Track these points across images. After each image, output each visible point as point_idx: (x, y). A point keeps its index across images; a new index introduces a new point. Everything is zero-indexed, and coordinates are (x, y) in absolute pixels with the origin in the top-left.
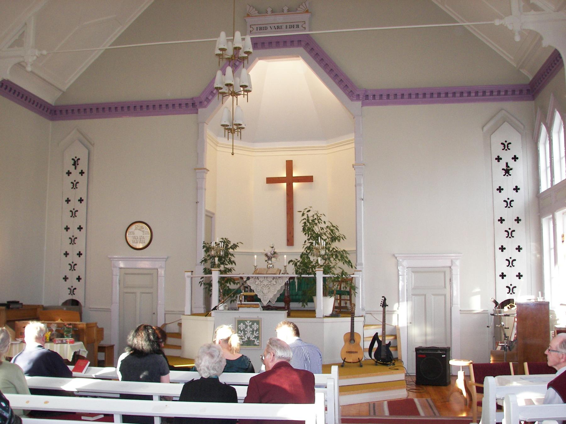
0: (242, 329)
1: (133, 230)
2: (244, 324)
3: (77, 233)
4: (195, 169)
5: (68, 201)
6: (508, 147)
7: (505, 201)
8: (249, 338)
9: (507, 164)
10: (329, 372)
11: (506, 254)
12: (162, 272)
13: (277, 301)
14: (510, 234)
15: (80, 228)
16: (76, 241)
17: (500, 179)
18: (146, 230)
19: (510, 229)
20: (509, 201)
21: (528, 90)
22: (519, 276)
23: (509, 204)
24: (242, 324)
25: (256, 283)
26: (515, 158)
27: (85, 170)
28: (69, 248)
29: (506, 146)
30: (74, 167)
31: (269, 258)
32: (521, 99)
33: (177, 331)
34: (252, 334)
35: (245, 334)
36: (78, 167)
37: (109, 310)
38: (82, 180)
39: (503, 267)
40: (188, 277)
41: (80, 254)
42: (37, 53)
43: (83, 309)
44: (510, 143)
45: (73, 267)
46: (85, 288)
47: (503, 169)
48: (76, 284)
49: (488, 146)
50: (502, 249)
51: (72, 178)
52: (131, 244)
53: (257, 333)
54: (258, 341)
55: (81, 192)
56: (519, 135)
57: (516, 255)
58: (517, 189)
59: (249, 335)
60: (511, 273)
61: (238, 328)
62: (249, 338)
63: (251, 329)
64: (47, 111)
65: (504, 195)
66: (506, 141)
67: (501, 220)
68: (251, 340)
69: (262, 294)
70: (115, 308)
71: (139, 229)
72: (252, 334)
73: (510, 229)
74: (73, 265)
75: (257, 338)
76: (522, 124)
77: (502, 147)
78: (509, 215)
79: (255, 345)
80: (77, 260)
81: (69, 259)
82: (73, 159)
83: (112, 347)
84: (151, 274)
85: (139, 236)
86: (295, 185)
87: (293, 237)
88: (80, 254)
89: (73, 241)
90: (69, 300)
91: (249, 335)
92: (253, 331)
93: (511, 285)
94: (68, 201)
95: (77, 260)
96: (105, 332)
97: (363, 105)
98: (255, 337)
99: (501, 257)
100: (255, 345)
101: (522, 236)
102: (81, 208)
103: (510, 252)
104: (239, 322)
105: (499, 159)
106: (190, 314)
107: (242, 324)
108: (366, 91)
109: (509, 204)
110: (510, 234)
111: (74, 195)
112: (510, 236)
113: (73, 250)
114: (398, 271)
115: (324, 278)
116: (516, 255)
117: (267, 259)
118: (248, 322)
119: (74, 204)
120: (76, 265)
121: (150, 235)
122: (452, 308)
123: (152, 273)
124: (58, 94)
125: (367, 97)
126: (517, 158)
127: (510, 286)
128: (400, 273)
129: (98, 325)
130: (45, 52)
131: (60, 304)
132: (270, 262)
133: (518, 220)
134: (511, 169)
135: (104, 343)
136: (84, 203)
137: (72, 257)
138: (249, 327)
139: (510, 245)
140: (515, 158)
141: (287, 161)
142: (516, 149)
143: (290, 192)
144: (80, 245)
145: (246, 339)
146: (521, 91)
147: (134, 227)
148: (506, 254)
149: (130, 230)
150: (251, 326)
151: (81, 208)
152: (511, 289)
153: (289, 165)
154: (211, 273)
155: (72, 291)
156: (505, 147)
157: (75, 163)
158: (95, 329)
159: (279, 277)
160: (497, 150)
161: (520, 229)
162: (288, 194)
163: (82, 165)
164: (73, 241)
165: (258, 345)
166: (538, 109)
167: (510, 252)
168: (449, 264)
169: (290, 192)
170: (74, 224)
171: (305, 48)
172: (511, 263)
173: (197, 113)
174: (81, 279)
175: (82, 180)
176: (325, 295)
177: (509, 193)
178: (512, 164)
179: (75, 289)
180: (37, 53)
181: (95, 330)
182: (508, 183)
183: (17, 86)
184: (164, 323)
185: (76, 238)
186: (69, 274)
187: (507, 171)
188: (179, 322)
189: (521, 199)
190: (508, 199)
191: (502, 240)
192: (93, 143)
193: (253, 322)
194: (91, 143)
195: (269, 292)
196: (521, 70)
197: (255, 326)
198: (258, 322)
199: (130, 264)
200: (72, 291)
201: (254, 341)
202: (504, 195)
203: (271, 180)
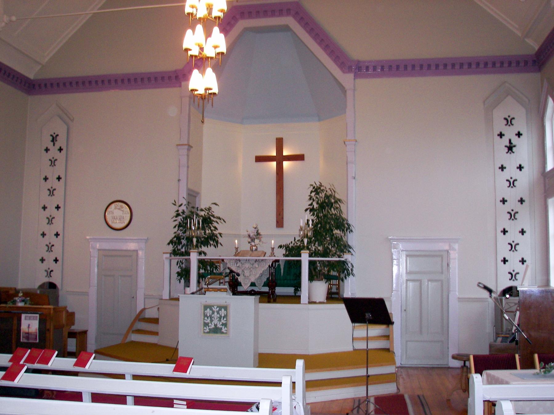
0: (208, 315)
2: (211, 309)
4: (177, 145)
5: (46, 179)
6: (513, 184)
7: (507, 180)
8: (216, 325)
9: (510, 141)
10: (293, 366)
11: (509, 238)
13: (263, 286)
14: (512, 216)
15: (58, 208)
16: (54, 221)
19: (512, 210)
21: (534, 62)
23: (512, 183)
24: (208, 310)
25: (238, 265)
26: (519, 135)
27: (64, 147)
29: (509, 121)
31: (253, 240)
32: (528, 72)
33: (156, 316)
34: (220, 320)
35: (211, 321)
36: (56, 143)
37: (86, 294)
38: (61, 157)
39: (504, 251)
40: (166, 258)
41: (57, 235)
42: (6, 18)
43: (61, 293)
44: (513, 118)
47: (506, 146)
48: (53, 266)
49: (489, 121)
50: (504, 232)
51: (50, 155)
52: (110, 223)
53: (225, 319)
54: (226, 329)
55: (59, 170)
56: (524, 110)
57: (519, 238)
58: (520, 168)
60: (514, 258)
61: (204, 313)
62: (216, 325)
63: (218, 315)
64: (16, 81)
65: (506, 174)
67: (504, 201)
68: (218, 328)
70: (93, 292)
71: (119, 209)
72: (220, 320)
74: (50, 246)
76: (526, 97)
78: (512, 195)
79: (223, 333)
80: (54, 240)
81: (46, 240)
82: (51, 135)
83: (85, 332)
84: (131, 256)
85: (119, 216)
86: (286, 164)
87: (283, 218)
88: (57, 235)
89: (50, 221)
91: (216, 321)
92: (220, 317)
93: (514, 271)
94: (46, 179)
95: (54, 240)
96: (77, 316)
97: (356, 77)
98: (223, 324)
99: (503, 241)
100: (223, 333)
101: (525, 219)
102: (59, 186)
103: (513, 236)
104: (206, 307)
105: (501, 135)
106: (168, 298)
107: (208, 310)
108: (359, 62)
109: (512, 183)
110: (512, 216)
113: (50, 231)
114: (392, 254)
116: (519, 238)
117: (250, 240)
118: (215, 307)
119: (53, 182)
120: (53, 245)
121: (129, 215)
123: (132, 255)
124: (38, 68)
125: (359, 68)
127: (512, 272)
128: (394, 257)
129: (67, 309)
130: (14, 18)
131: (36, 287)
132: (253, 244)
133: (522, 201)
134: (515, 146)
135: (77, 327)
136: (62, 181)
137: (50, 238)
138: (216, 313)
139: (513, 228)
140: (519, 135)
141: (277, 139)
142: (520, 125)
143: (280, 168)
144: (58, 226)
145: (213, 326)
146: (526, 63)
147: (113, 206)
148: (509, 238)
149: (109, 210)
150: (218, 313)
151: (59, 186)
152: (513, 276)
153: (280, 144)
154: (189, 255)
155: (49, 273)
157: (54, 139)
158: (64, 312)
159: (262, 260)
160: (500, 125)
161: (523, 211)
162: (277, 174)
163: (61, 142)
165: (226, 333)
166: (545, 80)
167: (513, 236)
169: (280, 168)
170: (51, 203)
172: (513, 247)
173: (180, 86)
176: (311, 278)
177: (511, 172)
179: (52, 271)
180: (6, 18)
181: (64, 315)
182: (511, 161)
183: (7, 67)
184: (143, 307)
185: (54, 218)
186: (46, 255)
187: (510, 148)
189: (525, 179)
192: (72, 118)
193: (220, 307)
194: (70, 119)
195: (252, 275)
196: (526, 40)
197: (223, 312)
198: (226, 308)
199: (106, 246)
200: (49, 273)
202: (506, 174)
203: (260, 159)
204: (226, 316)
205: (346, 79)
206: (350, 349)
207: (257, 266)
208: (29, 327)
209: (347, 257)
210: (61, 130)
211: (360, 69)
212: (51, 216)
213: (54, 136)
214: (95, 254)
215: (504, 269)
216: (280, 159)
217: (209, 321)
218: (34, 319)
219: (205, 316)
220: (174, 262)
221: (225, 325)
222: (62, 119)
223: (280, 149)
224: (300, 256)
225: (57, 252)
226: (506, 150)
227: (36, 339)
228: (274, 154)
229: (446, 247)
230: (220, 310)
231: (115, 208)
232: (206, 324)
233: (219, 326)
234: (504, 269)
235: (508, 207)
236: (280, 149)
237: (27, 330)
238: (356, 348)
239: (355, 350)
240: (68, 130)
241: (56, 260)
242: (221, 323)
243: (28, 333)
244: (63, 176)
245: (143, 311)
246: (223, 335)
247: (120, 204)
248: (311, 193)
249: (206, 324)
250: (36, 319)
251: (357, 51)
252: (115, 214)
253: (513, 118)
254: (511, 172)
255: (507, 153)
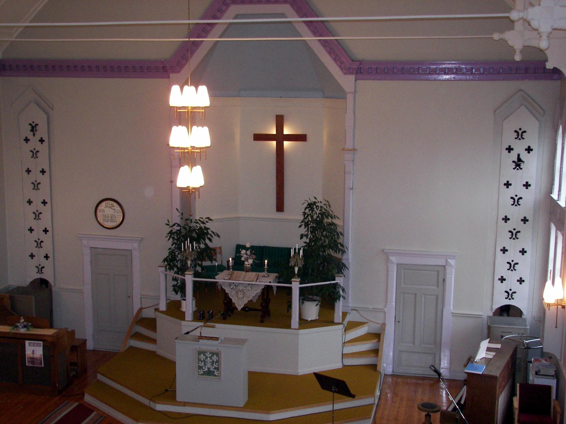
0: (202, 359)
1: (102, 208)
2: (204, 355)
3: (41, 207)
7: (512, 198)
8: (209, 369)
9: (519, 155)
11: (508, 257)
12: (136, 254)
14: (514, 234)
16: (40, 186)
17: (510, 173)
18: (117, 209)
19: (514, 229)
20: (516, 198)
22: (521, 281)
23: (516, 201)
24: (202, 355)
26: (523, 252)
27: (45, 138)
28: (33, 224)
29: (520, 135)
30: (32, 133)
34: (212, 365)
35: (205, 365)
36: (37, 133)
38: (43, 149)
39: (502, 270)
43: (54, 289)
45: (39, 244)
46: (53, 241)
47: (514, 162)
50: (504, 250)
55: (44, 193)
57: (518, 258)
58: (527, 185)
59: (209, 365)
61: (198, 358)
62: (209, 369)
65: (511, 192)
66: (520, 129)
67: (506, 219)
69: (236, 298)
70: (87, 288)
71: (110, 207)
72: (212, 365)
73: (514, 229)
74: (37, 213)
75: (217, 369)
77: (515, 135)
78: (516, 214)
79: (215, 376)
80: (43, 236)
81: (35, 236)
82: (30, 124)
86: (286, 144)
89: (37, 215)
90: (37, 279)
91: (209, 365)
92: (213, 362)
95: (43, 236)
98: (215, 368)
99: (502, 260)
100: (215, 376)
102: (44, 180)
103: (513, 255)
104: (200, 353)
105: (510, 149)
107: (202, 355)
109: (516, 201)
110: (514, 234)
111: (36, 165)
112: (514, 237)
113: (38, 227)
115: (301, 289)
116: (518, 258)
119: (36, 176)
120: (39, 183)
121: (121, 214)
122: (444, 310)
123: (127, 255)
126: (532, 150)
127: (509, 291)
136: (47, 174)
138: (209, 359)
140: (529, 150)
142: (530, 139)
143: (280, 147)
144: (45, 221)
145: (206, 369)
147: (104, 204)
148: (508, 257)
149: (100, 208)
150: (211, 358)
151: (44, 180)
153: (280, 122)
155: (40, 269)
156: (518, 135)
157: (33, 128)
160: (509, 139)
163: (42, 132)
164: (37, 215)
167: (513, 255)
168: (444, 264)
169: (280, 147)
171: (292, 5)
172: (512, 266)
173: (169, 78)
174: (49, 257)
175: (43, 149)
177: (517, 189)
178: (524, 156)
182: (518, 178)
186: (35, 251)
187: (518, 163)
188: (157, 307)
189: (529, 198)
190: (516, 196)
191: (505, 241)
192: (52, 106)
193: (213, 354)
197: (215, 358)
198: (217, 354)
200: (40, 269)
201: (214, 372)
202: (511, 192)
204: (217, 362)
205: (347, 81)
206: (339, 365)
207: (250, 289)
208: (33, 353)
209: (339, 280)
210: (40, 119)
211: (363, 70)
212: (37, 211)
213: (34, 125)
214: (87, 251)
215: (501, 288)
216: (280, 138)
217: (202, 364)
218: (38, 345)
219: (199, 360)
220: (170, 278)
221: (217, 369)
222: (38, 105)
223: (280, 128)
224: (291, 283)
225: (47, 247)
226: (513, 165)
227: (41, 363)
228: (274, 132)
229: (441, 262)
230: (213, 356)
231: (106, 207)
232: (200, 368)
233: (211, 369)
234: (501, 288)
235: (510, 226)
236: (280, 128)
237: (32, 356)
238: (345, 364)
239: (344, 366)
240: (48, 119)
241: (47, 257)
242: (213, 367)
243: (33, 358)
244: (47, 169)
245: (141, 309)
246: (216, 377)
247: (111, 202)
248: (305, 210)
249: (200, 368)
250: (40, 346)
251: (364, 44)
252: (106, 213)
253: (525, 132)
254: (517, 189)
255: (514, 169)
